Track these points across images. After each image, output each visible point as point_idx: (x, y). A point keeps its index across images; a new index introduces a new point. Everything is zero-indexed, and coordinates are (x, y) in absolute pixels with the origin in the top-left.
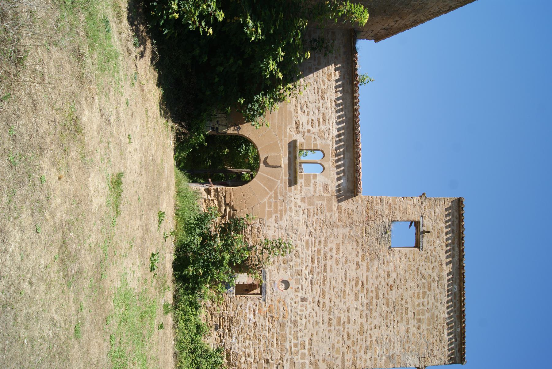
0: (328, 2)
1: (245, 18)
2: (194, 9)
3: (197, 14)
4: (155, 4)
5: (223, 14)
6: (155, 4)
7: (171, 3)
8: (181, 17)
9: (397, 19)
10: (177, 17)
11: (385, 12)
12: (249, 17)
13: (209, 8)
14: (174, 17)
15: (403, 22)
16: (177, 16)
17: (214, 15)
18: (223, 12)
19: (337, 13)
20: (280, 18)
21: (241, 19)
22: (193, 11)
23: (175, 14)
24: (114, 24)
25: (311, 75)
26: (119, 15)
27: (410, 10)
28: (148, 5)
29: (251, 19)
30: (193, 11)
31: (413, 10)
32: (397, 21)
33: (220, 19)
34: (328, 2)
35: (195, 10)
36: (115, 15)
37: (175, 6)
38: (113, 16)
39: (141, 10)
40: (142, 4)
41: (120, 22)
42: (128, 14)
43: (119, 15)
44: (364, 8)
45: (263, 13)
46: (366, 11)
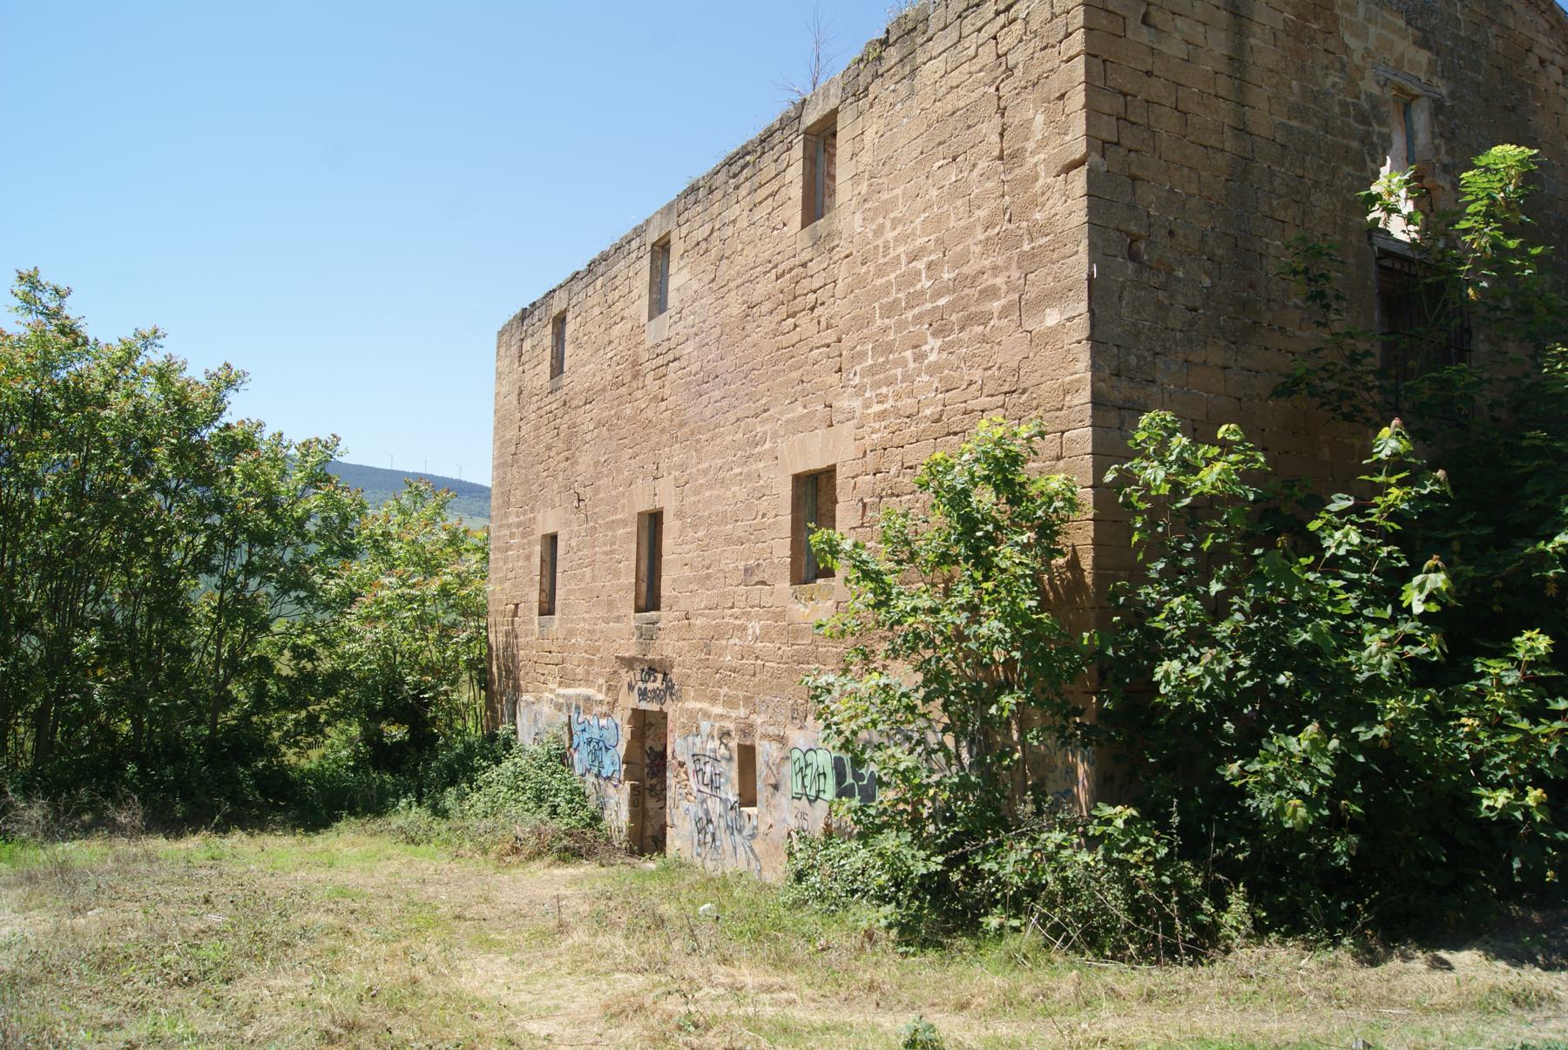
0: (1470, 291)
1: (1543, 559)
2: (1508, 734)
3: (1524, 724)
4: (1516, 864)
5: (1527, 634)
6: (1516, 864)
7: (1491, 808)
8: (1539, 780)
9: (1532, 62)
10: (1539, 792)
11: (1513, 109)
12: (1541, 545)
13: (1508, 682)
14: (1541, 805)
15: (1543, 40)
16: (1534, 796)
17: (1531, 665)
18: (1521, 635)
19: (1513, 253)
20: (1544, 440)
21: (1551, 573)
22: (1514, 738)
23: (1530, 801)
24: (1553, 1024)
25: (1080, 217)
26: (1522, 1000)
27: (1494, 30)
28: (1520, 888)
29: (1549, 538)
30: (1514, 738)
31: (1492, 22)
32: (1542, 61)
33: (1543, 643)
34: (1470, 291)
35: (1510, 731)
36: (1519, 1012)
37: (1502, 798)
38: (1521, 1020)
39: (1536, 917)
40: (1515, 909)
41: (1553, 999)
42: (1536, 964)
43: (1522, 1000)
44: (1473, 167)
45: (1533, 502)
46: (1483, 160)
